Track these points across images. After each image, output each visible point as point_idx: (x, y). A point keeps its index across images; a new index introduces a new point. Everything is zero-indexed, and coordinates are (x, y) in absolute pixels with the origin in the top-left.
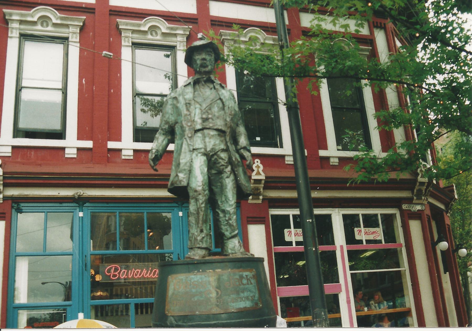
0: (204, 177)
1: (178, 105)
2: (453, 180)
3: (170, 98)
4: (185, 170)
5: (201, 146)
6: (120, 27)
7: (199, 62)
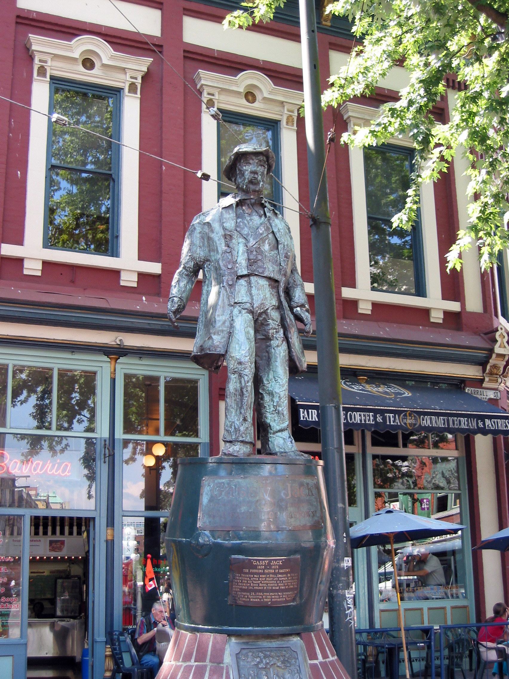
0: (250, 344)
1: (212, 235)
4: (222, 331)
5: (246, 299)
7: (247, 175)
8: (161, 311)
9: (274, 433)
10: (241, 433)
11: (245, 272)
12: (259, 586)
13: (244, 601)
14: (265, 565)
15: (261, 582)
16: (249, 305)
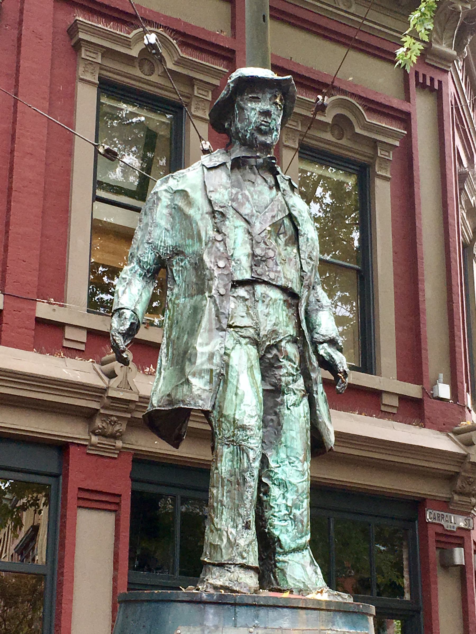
1: (191, 212)
3: (166, 191)
5: (246, 322)
8: (104, 329)
9: (286, 553)
11: (247, 276)
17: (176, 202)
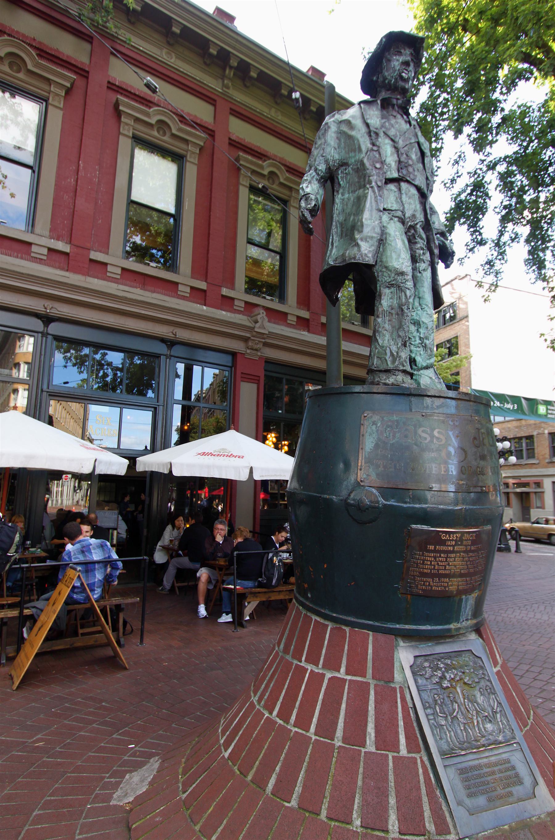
1: (353, 133)
2: (389, 363)
4: (372, 238)
5: (395, 207)
6: (121, 108)
10: (401, 360)
11: (395, 175)
12: (445, 569)
13: (422, 590)
14: (456, 541)
15: (449, 565)
16: (401, 213)
17: (341, 129)
